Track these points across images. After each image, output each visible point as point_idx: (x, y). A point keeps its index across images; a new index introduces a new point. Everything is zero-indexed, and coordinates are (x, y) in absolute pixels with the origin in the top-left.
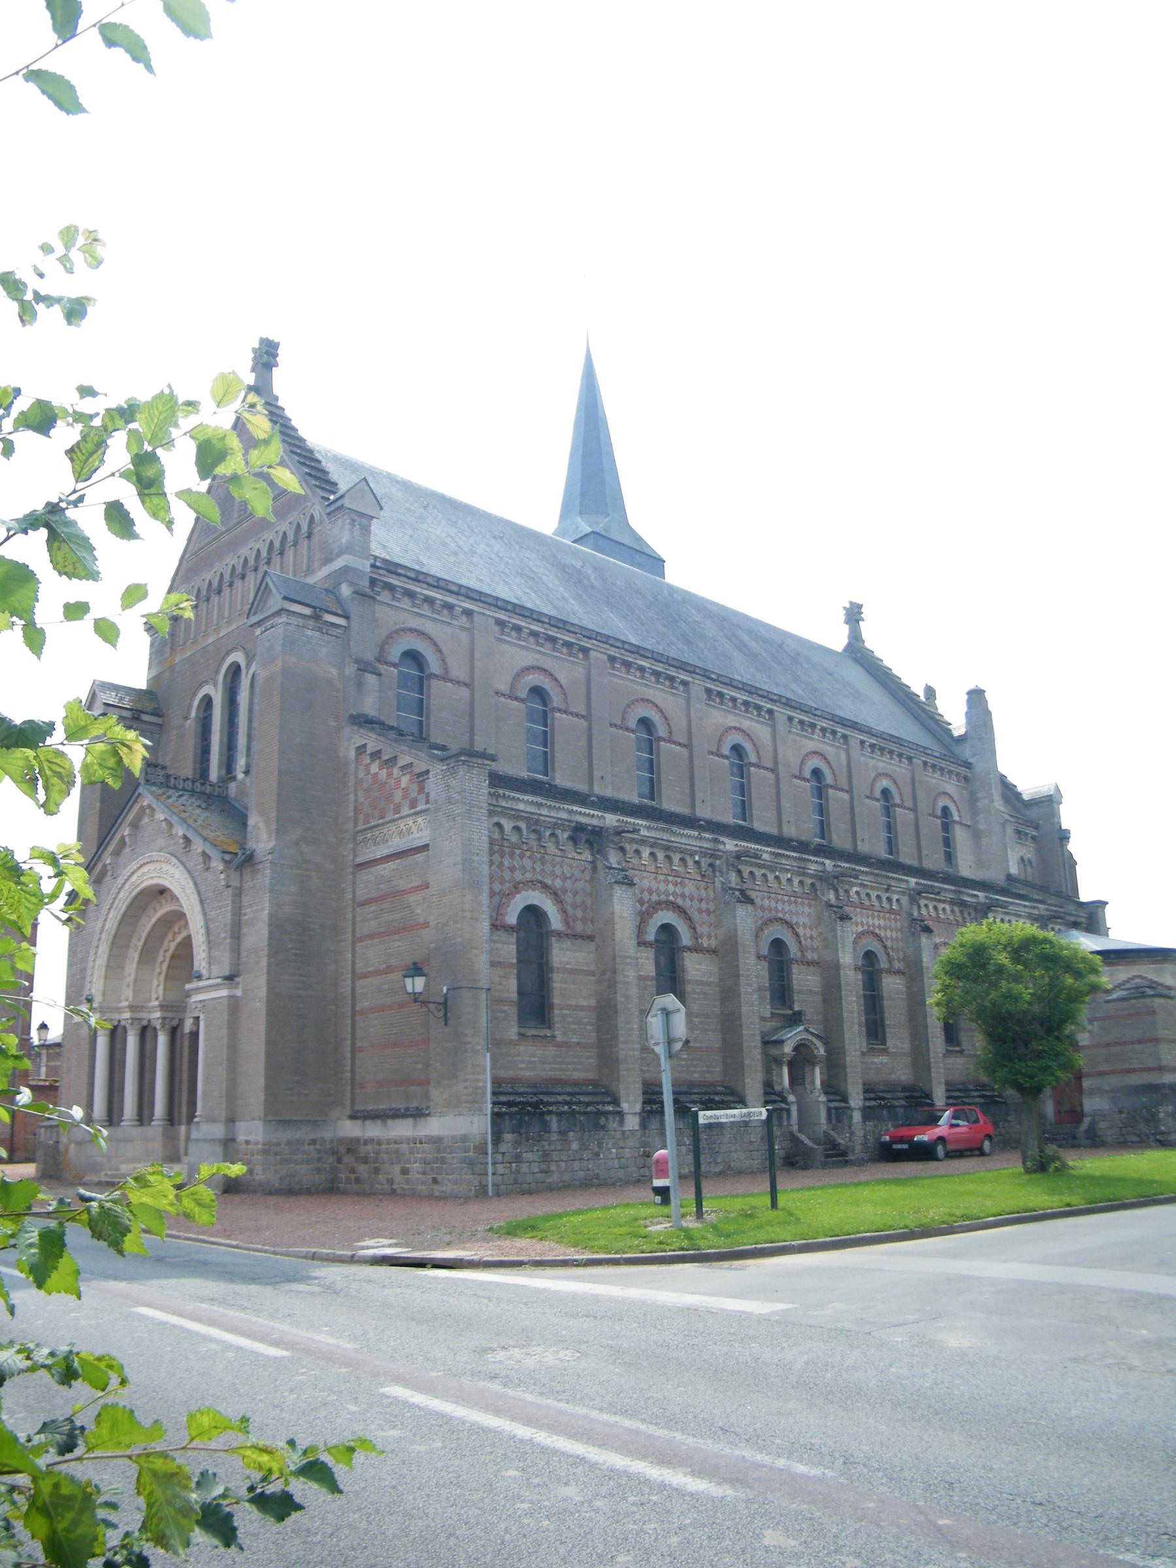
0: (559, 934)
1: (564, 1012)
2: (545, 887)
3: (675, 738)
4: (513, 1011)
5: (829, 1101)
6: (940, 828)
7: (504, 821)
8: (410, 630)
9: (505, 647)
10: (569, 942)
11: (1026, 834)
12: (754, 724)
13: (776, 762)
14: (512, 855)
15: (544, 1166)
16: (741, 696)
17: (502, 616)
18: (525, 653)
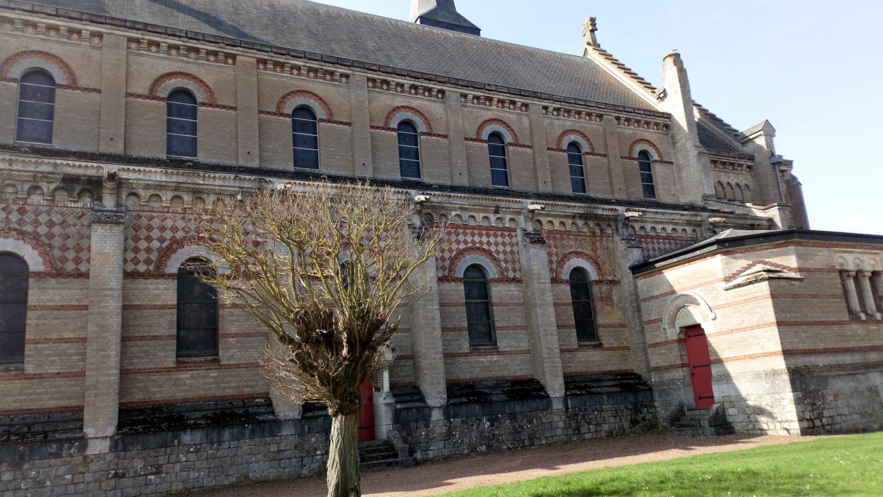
0: (38, 275)
1: (39, 346)
3: (596, 152)
5: (396, 402)
8: (33, 52)
10: (53, 281)
16: (407, 82)
17: (134, 34)
18: (167, 63)
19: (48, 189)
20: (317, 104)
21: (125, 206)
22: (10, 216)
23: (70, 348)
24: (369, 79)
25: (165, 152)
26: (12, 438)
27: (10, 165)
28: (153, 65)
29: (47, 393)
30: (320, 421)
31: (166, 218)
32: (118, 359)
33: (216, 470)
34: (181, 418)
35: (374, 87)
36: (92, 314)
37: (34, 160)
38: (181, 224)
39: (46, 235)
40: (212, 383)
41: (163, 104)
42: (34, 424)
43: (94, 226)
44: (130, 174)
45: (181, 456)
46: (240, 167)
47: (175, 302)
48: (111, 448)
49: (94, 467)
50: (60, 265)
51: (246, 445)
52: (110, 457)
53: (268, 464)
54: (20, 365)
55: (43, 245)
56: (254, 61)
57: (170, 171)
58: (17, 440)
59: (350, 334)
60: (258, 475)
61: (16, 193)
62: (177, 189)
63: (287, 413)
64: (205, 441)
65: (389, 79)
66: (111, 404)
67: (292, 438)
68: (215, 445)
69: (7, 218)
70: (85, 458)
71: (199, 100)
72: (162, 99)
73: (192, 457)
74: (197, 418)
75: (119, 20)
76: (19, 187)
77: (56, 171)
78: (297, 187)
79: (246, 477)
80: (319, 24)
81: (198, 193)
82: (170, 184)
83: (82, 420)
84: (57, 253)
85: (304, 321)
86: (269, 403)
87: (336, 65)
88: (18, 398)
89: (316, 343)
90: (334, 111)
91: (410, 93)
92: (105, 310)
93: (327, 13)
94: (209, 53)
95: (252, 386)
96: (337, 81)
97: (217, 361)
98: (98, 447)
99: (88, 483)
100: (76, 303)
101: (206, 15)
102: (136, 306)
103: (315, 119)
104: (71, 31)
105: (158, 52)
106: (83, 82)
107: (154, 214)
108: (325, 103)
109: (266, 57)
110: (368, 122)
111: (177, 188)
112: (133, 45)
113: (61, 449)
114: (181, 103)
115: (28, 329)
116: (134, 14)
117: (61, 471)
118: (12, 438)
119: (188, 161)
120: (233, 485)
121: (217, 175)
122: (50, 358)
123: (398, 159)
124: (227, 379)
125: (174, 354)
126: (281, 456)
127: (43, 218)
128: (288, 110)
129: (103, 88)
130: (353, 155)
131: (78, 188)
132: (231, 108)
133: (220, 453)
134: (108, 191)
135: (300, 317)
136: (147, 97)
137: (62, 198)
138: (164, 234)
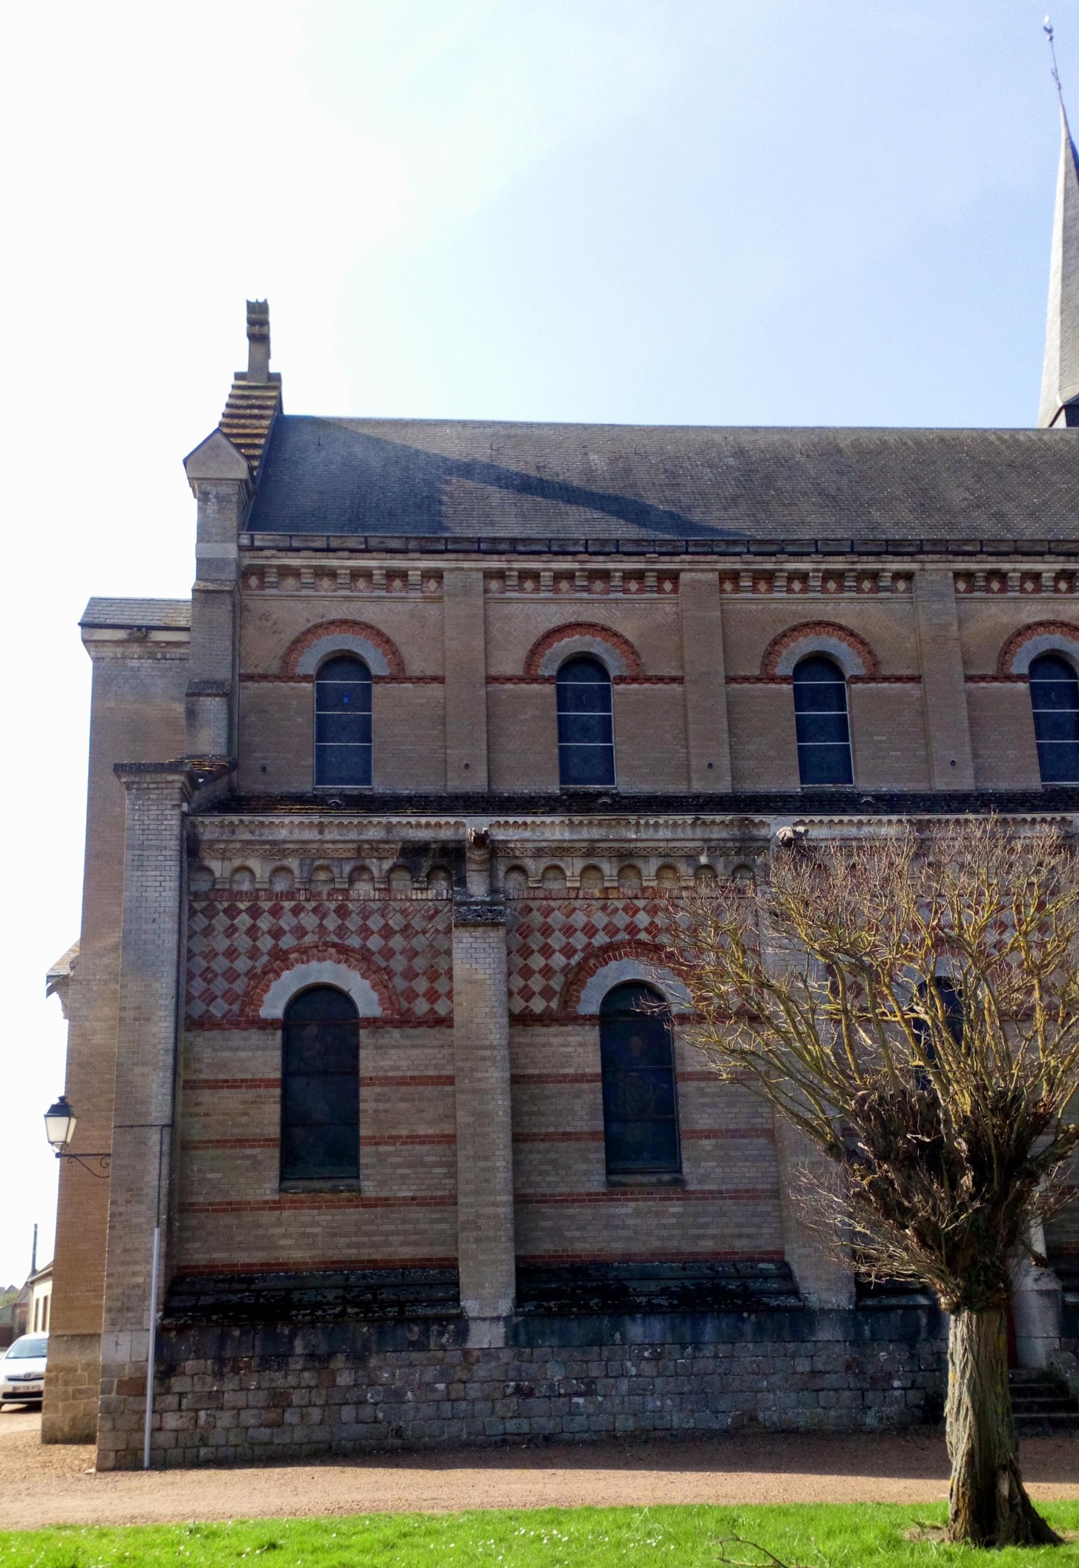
2: (344, 952)
4: (271, 1159)
5: (1066, 1290)
7: (254, 864)
8: (333, 623)
9: (513, 609)
10: (396, 1033)
14: (276, 912)
15: (272, 1416)
16: (1048, 567)
17: (495, 563)
18: (553, 608)
19: (381, 870)
20: (844, 645)
21: (504, 892)
22: (325, 922)
23: (429, 1154)
24: (957, 575)
25: (557, 780)
26: (349, 1310)
27: (321, 833)
28: (532, 614)
29: (397, 1233)
30: (896, 1317)
31: (575, 909)
32: (509, 1175)
33: (693, 1397)
34: (623, 1291)
35: (970, 589)
36: (462, 1092)
37: (356, 821)
38: (600, 919)
39: (380, 952)
40: (674, 1226)
41: (550, 689)
42: (381, 1287)
43: (456, 933)
44: (513, 831)
45: (629, 1364)
46: (697, 797)
47: (598, 1070)
48: (506, 1338)
49: (481, 1371)
50: (405, 1005)
51: (749, 1354)
52: (506, 1356)
53: (793, 1396)
54: (354, 1182)
55: (379, 969)
56: (714, 577)
57: (576, 819)
58: (357, 1314)
59: (975, 1143)
60: (775, 1418)
61: (332, 880)
62: (590, 852)
63: (824, 1296)
64: (669, 1339)
65: (1005, 566)
66: (503, 1257)
67: (838, 1348)
68: (689, 1350)
69: (321, 925)
70: (466, 1353)
71: (613, 673)
72: (547, 680)
73: (648, 1368)
74: (650, 1294)
75: (469, 540)
76: (336, 870)
77: (391, 838)
78: (821, 829)
79: (753, 1419)
80: (841, 473)
81: (627, 859)
82: (578, 845)
83: (457, 1284)
84: (400, 983)
85: (878, 1116)
86: (786, 1273)
87: (884, 557)
88: (354, 1239)
89: (907, 1162)
90: (882, 654)
91: (1057, 590)
92: (482, 1085)
93: (856, 445)
94: (628, 576)
95: (749, 1236)
96: (886, 589)
97: (679, 1182)
98: (486, 1336)
99: (474, 1401)
100: (432, 1072)
101: (617, 499)
102: (531, 1076)
103: (842, 678)
104: (391, 575)
105: (537, 590)
106: (416, 666)
107: (553, 904)
108: (862, 642)
109: (738, 566)
110: (960, 668)
111: (591, 850)
112: (494, 585)
113: (426, 1333)
114: (582, 684)
115: (363, 1118)
116: (492, 524)
117: (429, 1376)
118: (349, 1310)
119: (600, 794)
120: (727, 1431)
121: (661, 821)
122: (399, 1171)
123: (1034, 742)
124: (701, 1220)
125: (601, 1168)
126: (819, 1383)
127: (375, 923)
128: (785, 666)
129: (447, 674)
130: (927, 745)
131: (426, 865)
132: (673, 680)
133: (700, 1365)
134: (474, 867)
135: (871, 1108)
136: (522, 680)
137: (402, 883)
138: (571, 940)
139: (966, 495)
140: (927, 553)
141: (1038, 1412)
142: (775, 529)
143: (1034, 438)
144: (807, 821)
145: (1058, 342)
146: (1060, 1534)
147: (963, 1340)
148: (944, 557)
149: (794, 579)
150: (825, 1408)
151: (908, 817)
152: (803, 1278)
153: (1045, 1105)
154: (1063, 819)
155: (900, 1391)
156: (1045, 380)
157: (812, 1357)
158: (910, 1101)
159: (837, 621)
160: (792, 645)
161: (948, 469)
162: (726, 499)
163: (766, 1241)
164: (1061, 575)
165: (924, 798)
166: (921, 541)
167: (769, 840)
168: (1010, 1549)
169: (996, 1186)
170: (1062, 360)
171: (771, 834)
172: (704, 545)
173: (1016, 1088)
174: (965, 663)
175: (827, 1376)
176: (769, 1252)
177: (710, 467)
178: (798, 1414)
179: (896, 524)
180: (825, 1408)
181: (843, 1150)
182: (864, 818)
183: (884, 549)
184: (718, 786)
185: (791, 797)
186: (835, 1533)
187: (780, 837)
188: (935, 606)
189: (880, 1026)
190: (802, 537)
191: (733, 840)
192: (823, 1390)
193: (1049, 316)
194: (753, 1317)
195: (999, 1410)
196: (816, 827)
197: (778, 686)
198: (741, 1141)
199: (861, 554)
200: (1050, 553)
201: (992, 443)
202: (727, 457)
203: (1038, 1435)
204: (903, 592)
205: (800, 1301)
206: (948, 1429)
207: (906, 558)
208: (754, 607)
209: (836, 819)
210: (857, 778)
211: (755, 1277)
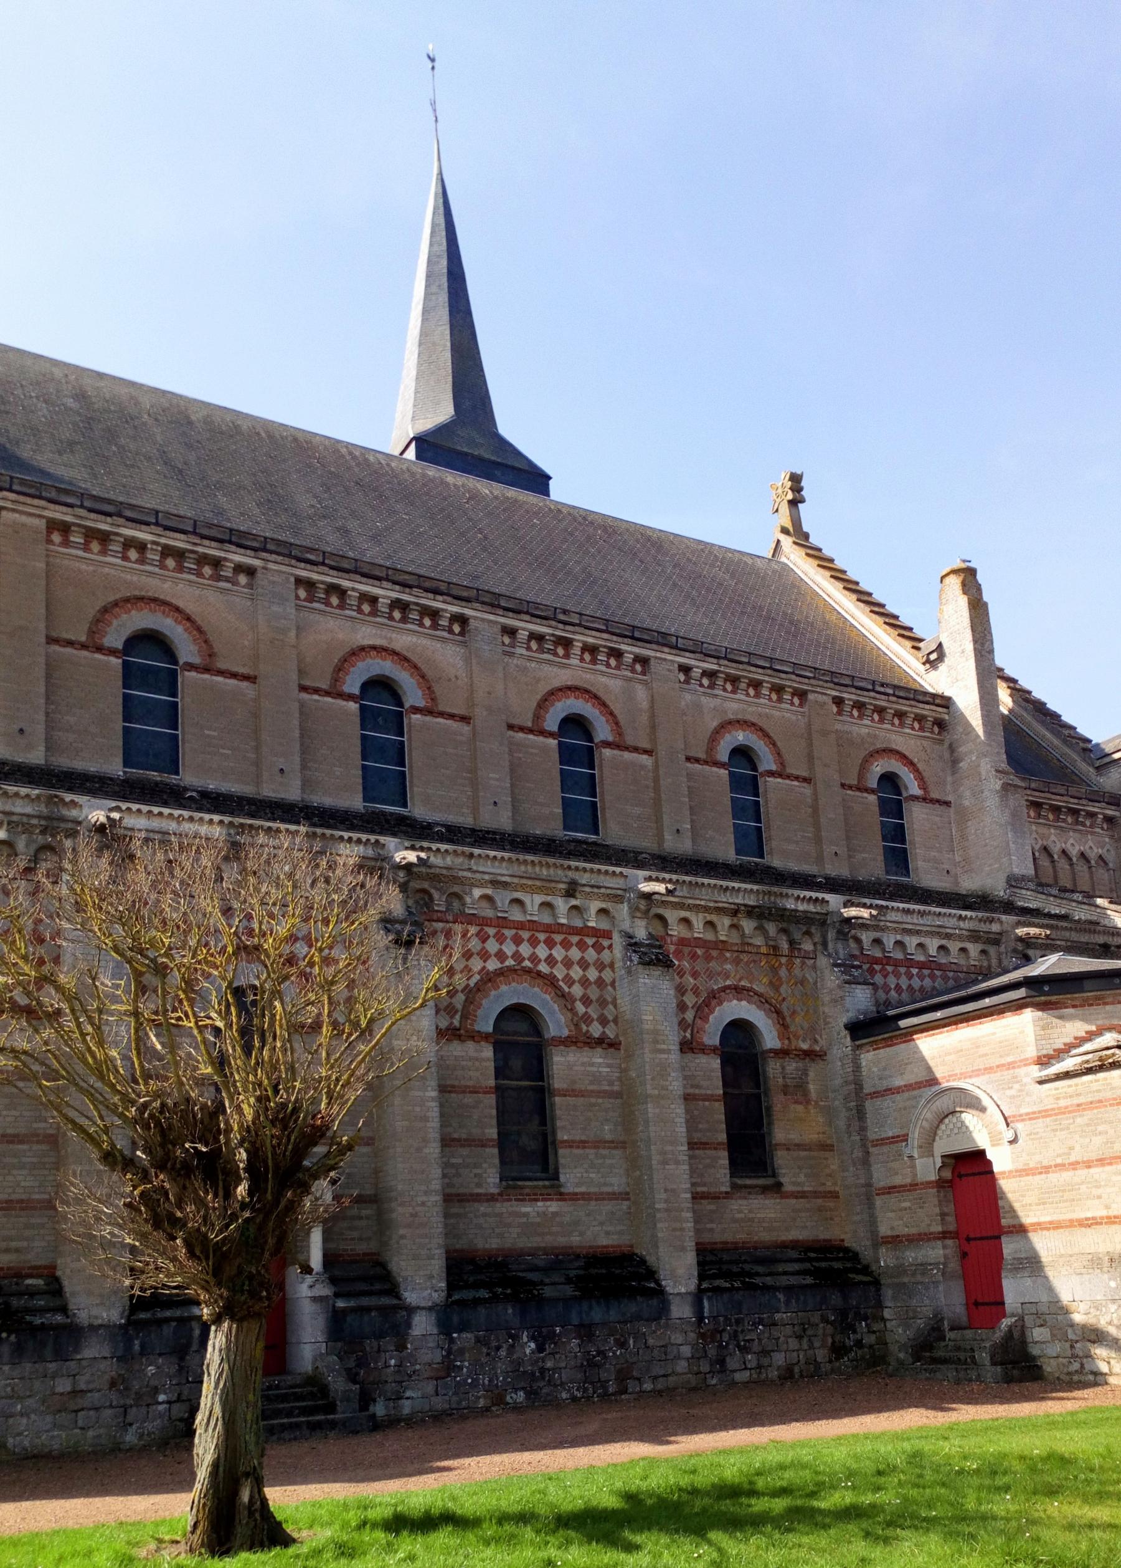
3: (789, 771)
5: (337, 1295)
6: (556, 756)
11: (1092, 815)
12: (425, 642)
13: (653, 739)
16: (386, 593)
24: (299, 581)
30: (168, 1330)
35: (311, 599)
56: (41, 524)
60: (26, 1443)
65: (346, 584)
67: (103, 1365)
78: (138, 819)
85: (158, 1123)
86: (55, 1288)
87: (227, 546)
89: (182, 1172)
90: (217, 647)
93: (208, 421)
103: (176, 663)
108: (199, 629)
109: (69, 519)
110: (294, 676)
123: (359, 762)
128: (115, 638)
130: (257, 749)
135: (151, 1116)
139: (314, 502)
140: (271, 552)
141: (298, 1416)
142: (114, 489)
143: (383, 462)
144: (124, 808)
145: (414, 373)
146: (295, 1535)
147: (220, 1351)
148: (287, 560)
149: (131, 546)
150: (82, 1428)
151: (230, 819)
152: (73, 1294)
153: (323, 1117)
154: (377, 841)
155: (165, 1406)
156: (400, 407)
157: (74, 1376)
158: (193, 1109)
159: (174, 601)
160: (125, 616)
161: (298, 471)
162: (61, 441)
163: (36, 1256)
164: (396, 604)
165: (251, 801)
166: (266, 538)
167: (80, 823)
168: (244, 1555)
169: (269, 1196)
170: (416, 392)
171: (83, 816)
172: (32, 487)
173: (297, 1099)
174: (301, 672)
175: (89, 1395)
176: (39, 1267)
177: (45, 402)
178: (53, 1437)
179: (242, 514)
180: (82, 1428)
181: (119, 1158)
182: (186, 814)
183: (227, 537)
184: (28, 756)
185: (111, 779)
186: (66, 1559)
187: (93, 820)
188: (275, 608)
189: (171, 1032)
190: (143, 504)
191: (39, 817)
192: (82, 1409)
193: (409, 345)
194: (13, 1338)
195: (249, 1417)
196: (133, 816)
197: (105, 658)
198: (20, 1147)
199: (203, 537)
200: (387, 580)
201: (343, 456)
202: (66, 396)
203: (295, 1439)
204: (243, 587)
205: (68, 1317)
206: (196, 1441)
207: (249, 552)
208: (84, 567)
209: (156, 810)
210: (184, 770)
211: (21, 1294)
